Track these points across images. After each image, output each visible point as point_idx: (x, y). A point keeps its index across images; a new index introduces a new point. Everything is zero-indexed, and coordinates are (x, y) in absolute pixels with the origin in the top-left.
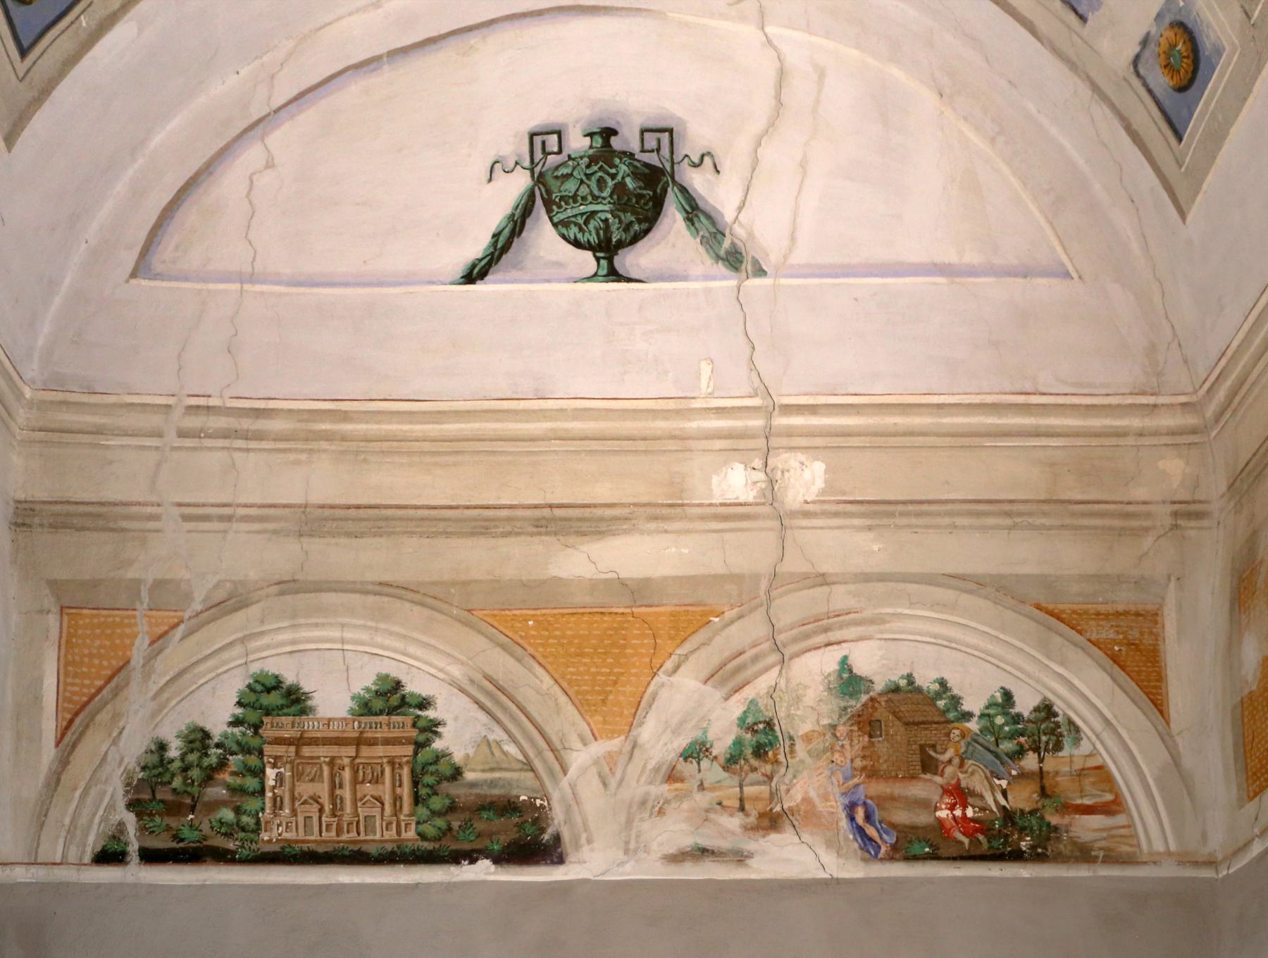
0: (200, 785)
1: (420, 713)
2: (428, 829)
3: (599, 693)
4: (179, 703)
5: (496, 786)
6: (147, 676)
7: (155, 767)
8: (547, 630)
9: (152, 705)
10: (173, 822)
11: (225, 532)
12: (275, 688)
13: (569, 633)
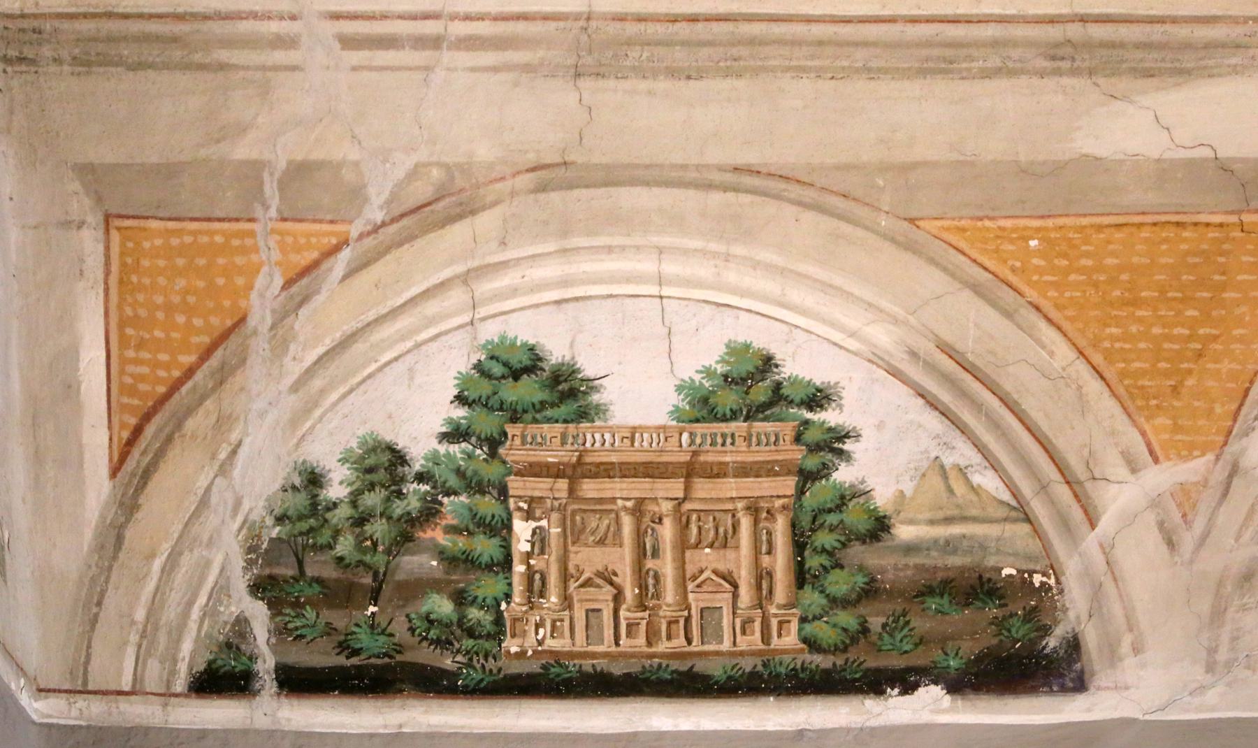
0: (388, 552)
1: (809, 415)
2: (824, 631)
3: (1166, 374)
4: (344, 396)
5: (955, 552)
6: (280, 345)
7: (301, 518)
8: (1065, 256)
9: (292, 401)
10: (339, 619)
11: (428, 69)
12: (530, 369)
13: (1110, 261)
